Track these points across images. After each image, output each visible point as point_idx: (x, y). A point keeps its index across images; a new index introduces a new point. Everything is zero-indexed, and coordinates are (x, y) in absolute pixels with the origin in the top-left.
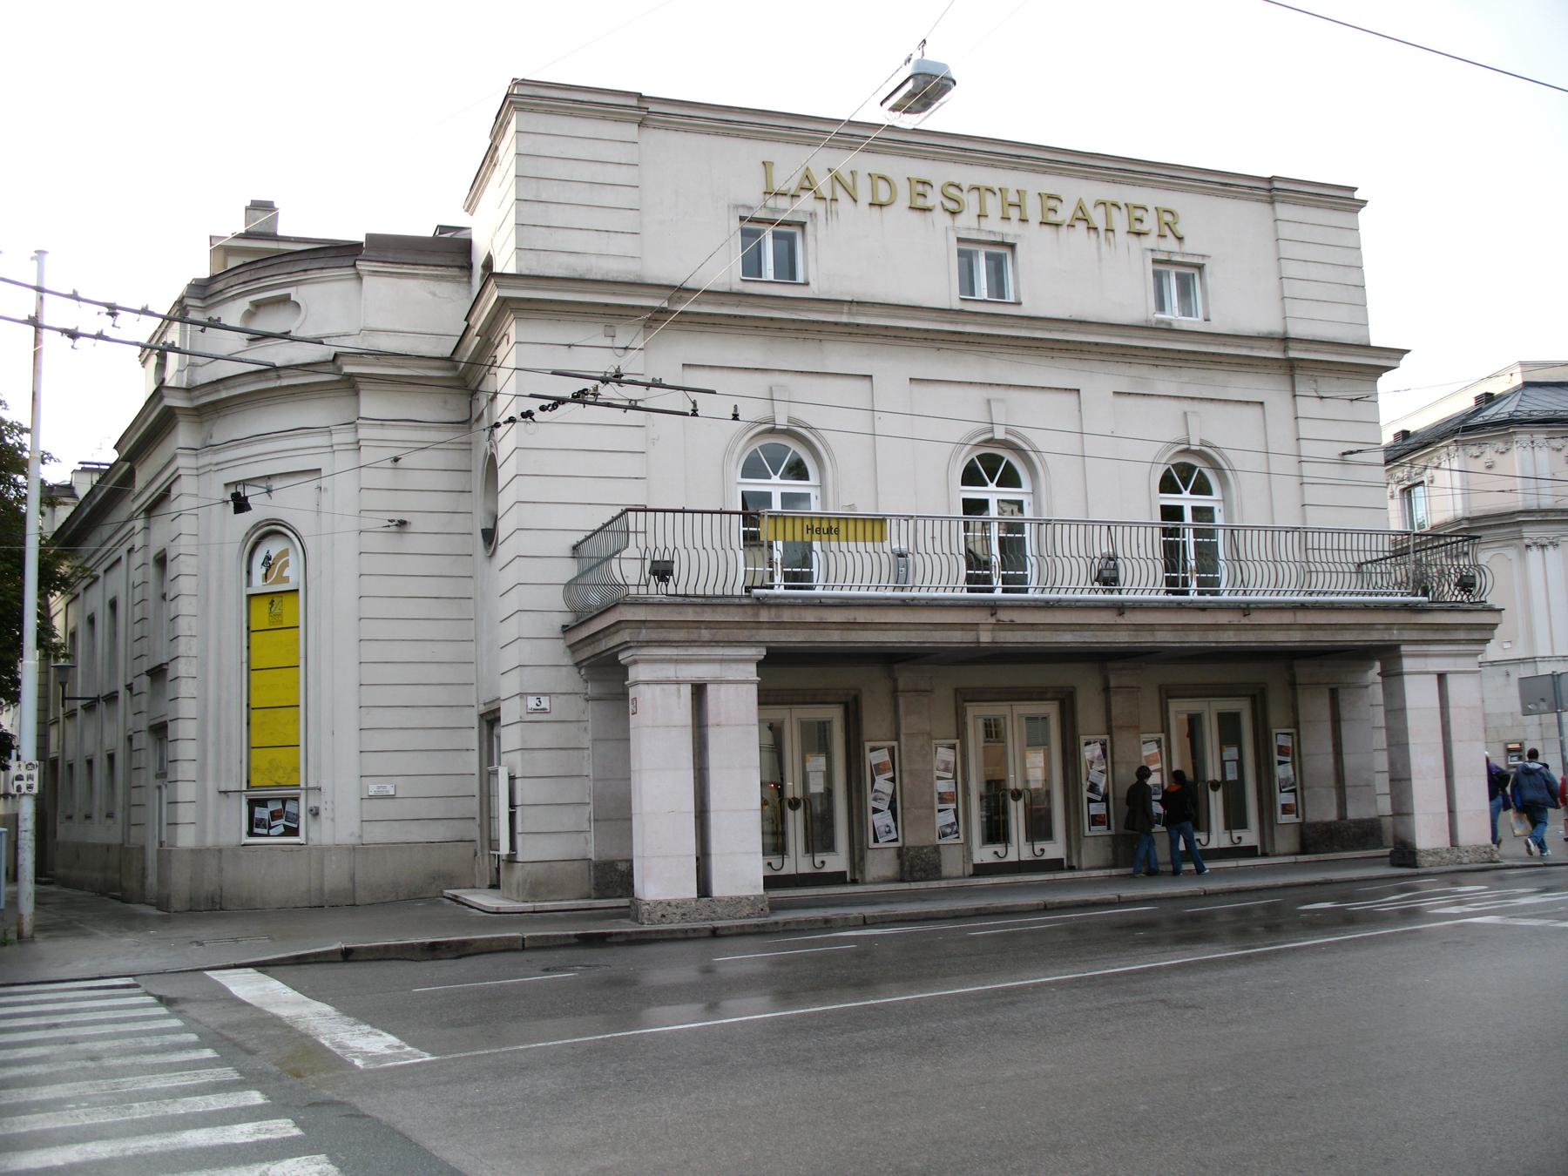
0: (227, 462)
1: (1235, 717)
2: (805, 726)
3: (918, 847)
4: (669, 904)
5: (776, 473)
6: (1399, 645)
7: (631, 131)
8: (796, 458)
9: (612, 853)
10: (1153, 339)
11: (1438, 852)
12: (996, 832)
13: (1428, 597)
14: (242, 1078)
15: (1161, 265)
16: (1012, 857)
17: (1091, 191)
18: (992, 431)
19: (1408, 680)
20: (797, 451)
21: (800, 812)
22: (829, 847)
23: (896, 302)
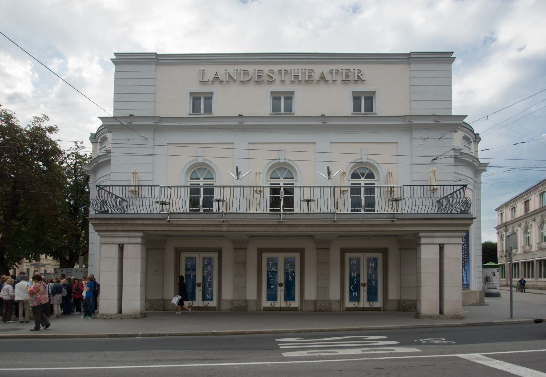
0: (103, 181)
1: (375, 260)
2: (369, 260)
4: (106, 315)
5: (363, 177)
6: (418, 233)
7: (153, 67)
8: (370, 172)
10: (427, 120)
11: (432, 317)
12: (272, 297)
15: (356, 98)
17: (325, 69)
18: (362, 159)
19: (423, 248)
20: (370, 169)
22: (293, 299)
23: (302, 115)
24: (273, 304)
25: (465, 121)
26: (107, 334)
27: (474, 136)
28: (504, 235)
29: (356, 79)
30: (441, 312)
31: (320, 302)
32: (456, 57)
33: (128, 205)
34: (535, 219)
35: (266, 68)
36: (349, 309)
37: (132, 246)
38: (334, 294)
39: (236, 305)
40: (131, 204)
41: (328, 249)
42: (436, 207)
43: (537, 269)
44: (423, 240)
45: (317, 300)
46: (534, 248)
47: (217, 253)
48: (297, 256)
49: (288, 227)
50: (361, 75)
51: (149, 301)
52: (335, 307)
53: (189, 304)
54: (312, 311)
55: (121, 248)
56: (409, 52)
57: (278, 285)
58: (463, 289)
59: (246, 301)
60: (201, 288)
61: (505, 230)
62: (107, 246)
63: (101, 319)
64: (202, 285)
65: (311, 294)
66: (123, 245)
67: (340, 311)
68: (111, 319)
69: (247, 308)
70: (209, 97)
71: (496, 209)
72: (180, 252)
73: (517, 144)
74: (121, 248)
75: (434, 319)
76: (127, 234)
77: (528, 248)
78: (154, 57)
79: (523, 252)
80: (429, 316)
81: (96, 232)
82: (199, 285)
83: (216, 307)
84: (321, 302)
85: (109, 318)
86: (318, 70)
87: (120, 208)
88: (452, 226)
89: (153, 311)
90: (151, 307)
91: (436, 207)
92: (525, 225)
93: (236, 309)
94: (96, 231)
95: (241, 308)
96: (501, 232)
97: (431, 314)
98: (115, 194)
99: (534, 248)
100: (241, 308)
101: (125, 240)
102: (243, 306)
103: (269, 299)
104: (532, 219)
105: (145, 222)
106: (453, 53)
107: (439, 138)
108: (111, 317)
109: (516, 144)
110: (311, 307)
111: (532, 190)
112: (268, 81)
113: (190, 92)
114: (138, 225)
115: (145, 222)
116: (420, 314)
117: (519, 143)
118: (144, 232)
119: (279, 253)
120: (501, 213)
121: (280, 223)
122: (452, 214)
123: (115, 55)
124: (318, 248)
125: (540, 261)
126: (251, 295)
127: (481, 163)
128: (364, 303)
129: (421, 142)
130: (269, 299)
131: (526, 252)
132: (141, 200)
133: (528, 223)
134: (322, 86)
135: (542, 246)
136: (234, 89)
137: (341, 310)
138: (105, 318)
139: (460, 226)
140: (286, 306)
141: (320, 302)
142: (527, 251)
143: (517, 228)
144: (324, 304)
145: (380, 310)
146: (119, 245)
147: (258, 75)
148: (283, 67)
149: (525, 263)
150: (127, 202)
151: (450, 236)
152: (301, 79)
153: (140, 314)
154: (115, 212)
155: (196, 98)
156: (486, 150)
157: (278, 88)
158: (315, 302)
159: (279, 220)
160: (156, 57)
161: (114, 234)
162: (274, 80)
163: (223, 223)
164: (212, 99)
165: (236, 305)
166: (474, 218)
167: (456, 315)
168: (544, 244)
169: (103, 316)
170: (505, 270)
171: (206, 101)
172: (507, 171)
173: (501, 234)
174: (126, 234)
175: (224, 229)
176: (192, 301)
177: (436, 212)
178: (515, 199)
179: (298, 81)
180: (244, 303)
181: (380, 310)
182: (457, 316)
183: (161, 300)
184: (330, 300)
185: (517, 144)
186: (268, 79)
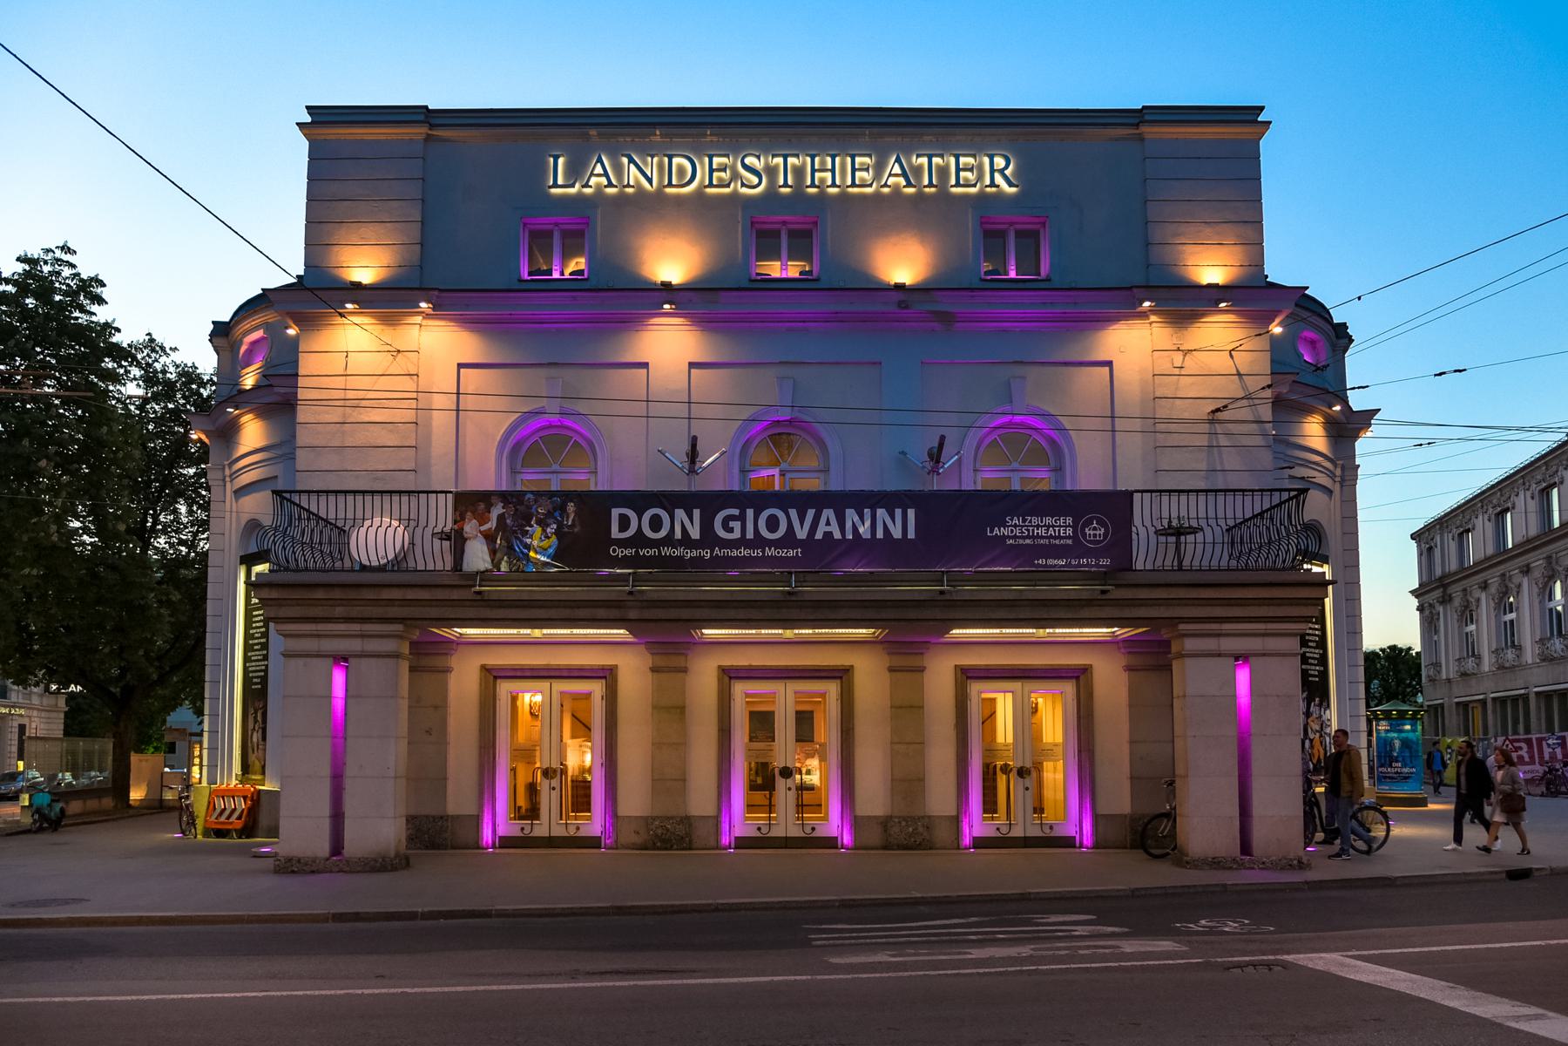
11: (1219, 862)
25: (1306, 292)
26: (332, 911)
27: (1332, 334)
28: (1439, 614)
30: (1246, 847)
31: (900, 822)
32: (1270, 122)
34: (1486, 582)
37: (373, 661)
39: (659, 831)
42: (1226, 546)
43: (1539, 719)
45: (891, 817)
46: (1530, 654)
54: (877, 849)
56: (1140, 107)
58: (775, 693)
59: (687, 820)
61: (1441, 599)
62: (301, 662)
63: (283, 873)
68: (313, 872)
69: (690, 841)
71: (1412, 535)
73: (1444, 373)
75: (1224, 868)
77: (1510, 654)
78: (422, 117)
79: (1498, 669)
80: (1210, 860)
83: (600, 837)
84: (904, 823)
91: (1226, 546)
92: (1500, 584)
93: (659, 844)
95: (674, 841)
96: (1431, 606)
97: (1217, 855)
98: (316, 513)
99: (1530, 654)
100: (674, 841)
104: (1519, 568)
105: (411, 594)
106: (1262, 109)
108: (313, 869)
109: (1440, 374)
111: (1517, 477)
116: (1187, 856)
120: (1427, 546)
121: (788, 598)
123: (311, 111)
125: (1546, 697)
127: (1354, 410)
131: (1506, 668)
133: (1510, 580)
135: (1553, 648)
138: (296, 869)
139: (1292, 605)
141: (900, 822)
142: (1507, 665)
143: (1477, 593)
144: (911, 829)
149: (1502, 701)
150: (344, 531)
151: (1263, 631)
156: (1359, 388)
160: (427, 117)
161: (321, 627)
163: (630, 598)
165: (659, 831)
167: (1286, 859)
168: (1557, 645)
169: (289, 864)
170: (1447, 722)
172: (1421, 445)
173: (1431, 612)
174: (356, 627)
178: (1466, 507)
180: (681, 826)
182: (1291, 860)
184: (929, 817)
185: (1444, 373)
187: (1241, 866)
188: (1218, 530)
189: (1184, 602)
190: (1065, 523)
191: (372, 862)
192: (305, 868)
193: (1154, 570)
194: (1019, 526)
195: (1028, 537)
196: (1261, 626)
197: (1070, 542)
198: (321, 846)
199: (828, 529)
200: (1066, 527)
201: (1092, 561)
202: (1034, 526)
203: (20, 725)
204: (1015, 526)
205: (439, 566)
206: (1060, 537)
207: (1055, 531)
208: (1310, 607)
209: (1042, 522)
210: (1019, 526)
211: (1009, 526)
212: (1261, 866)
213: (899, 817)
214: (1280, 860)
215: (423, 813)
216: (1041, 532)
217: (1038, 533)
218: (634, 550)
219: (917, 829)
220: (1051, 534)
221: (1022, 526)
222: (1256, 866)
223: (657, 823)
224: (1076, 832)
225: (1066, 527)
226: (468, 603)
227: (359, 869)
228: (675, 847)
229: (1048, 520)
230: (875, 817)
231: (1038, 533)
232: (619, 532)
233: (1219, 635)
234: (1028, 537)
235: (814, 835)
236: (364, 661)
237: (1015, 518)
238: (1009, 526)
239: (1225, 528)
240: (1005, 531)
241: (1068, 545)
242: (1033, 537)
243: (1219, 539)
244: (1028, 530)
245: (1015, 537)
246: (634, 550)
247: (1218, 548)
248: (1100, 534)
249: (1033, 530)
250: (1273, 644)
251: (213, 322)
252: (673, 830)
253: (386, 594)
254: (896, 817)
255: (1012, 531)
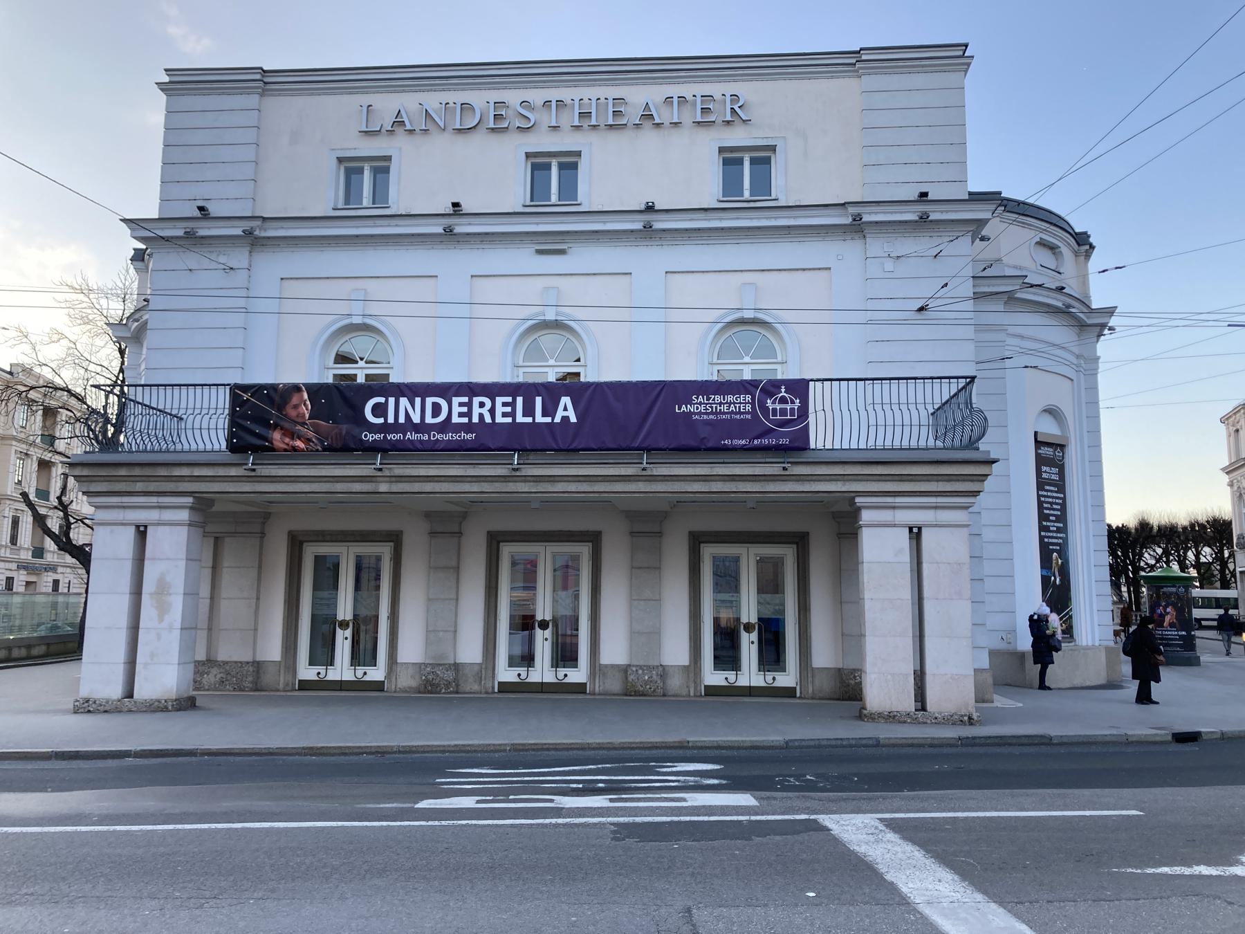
2: (761, 562)
3: (241, 662)
7: (253, 100)
9: (851, 664)
11: (895, 716)
12: (727, 656)
13: (309, 419)
14: (616, 829)
15: (730, 159)
16: (743, 681)
21: (548, 633)
22: (373, 662)
24: (523, 676)
29: (729, 118)
31: (637, 670)
33: (183, 427)
35: (513, 97)
36: (712, 691)
37: (167, 528)
38: (675, 652)
40: (189, 425)
41: (659, 534)
44: (866, 516)
45: (629, 665)
47: (590, 544)
48: (385, 550)
49: (534, 481)
50: (739, 107)
51: (220, 665)
52: (675, 683)
53: (319, 673)
54: (618, 695)
55: (142, 533)
57: (742, 627)
59: (457, 667)
60: (348, 633)
64: (351, 625)
65: (615, 651)
66: (146, 527)
67: (690, 695)
68: (106, 711)
69: (457, 685)
70: (382, 167)
72: (498, 542)
73: (1106, 270)
74: (142, 533)
75: (900, 722)
76: (156, 501)
78: (258, 77)
81: (85, 498)
82: (344, 625)
83: (586, 683)
84: (640, 672)
85: (102, 708)
86: (639, 95)
87: (155, 433)
88: (937, 481)
89: (230, 691)
90: (223, 682)
94: (84, 493)
97: (893, 710)
98: (149, 404)
101: (153, 515)
102: (447, 681)
103: (512, 663)
105: (197, 472)
107: (935, 256)
108: (107, 708)
109: (1104, 271)
110: (614, 684)
112: (518, 127)
113: (526, 153)
114: (181, 478)
115: (197, 472)
117: (1112, 269)
118: (197, 495)
119: (542, 544)
122: (140, 452)
124: (840, 534)
126: (470, 651)
128: (750, 674)
129: (889, 265)
130: (512, 663)
132: (199, 417)
134: (649, 136)
136: (441, 146)
137: (692, 694)
138: (92, 709)
139: (958, 480)
140: (555, 681)
144: (646, 678)
145: (794, 696)
146: (138, 527)
147: (702, 109)
148: (554, 94)
150: (181, 419)
151: (935, 505)
152: (556, 123)
153: (176, 700)
154: (139, 446)
155: (351, 167)
157: (737, 137)
158: (625, 670)
159: (510, 466)
161: (126, 499)
162: (534, 124)
163: (379, 474)
164: (389, 173)
165: (430, 677)
166: (994, 462)
171: (561, 171)
175: (383, 487)
176: (526, 669)
177: (931, 443)
179: (653, 124)
181: (794, 696)
182: (962, 716)
183: (248, 663)
185: (1106, 270)
186: (518, 124)
187: (916, 721)
188: (924, 413)
189: (860, 477)
190: (745, 400)
191: (157, 703)
192: (99, 708)
193: (867, 449)
194: (703, 404)
195: (712, 413)
196: (933, 500)
197: (749, 417)
198: (114, 691)
199: (565, 414)
200: (746, 403)
201: (772, 441)
202: (717, 404)
203: (54, 580)
204: (700, 404)
205: (217, 447)
206: (740, 413)
207: (735, 407)
208: (976, 483)
209: (724, 400)
210: (704, 403)
211: (695, 404)
212: (933, 721)
213: (637, 666)
214: (952, 716)
215: (235, 659)
216: (724, 408)
217: (720, 410)
218: (382, 435)
219: (652, 677)
220: (732, 410)
221: (707, 404)
222: (929, 722)
223: (429, 669)
224: (797, 685)
225: (746, 403)
226: (244, 479)
227: (144, 709)
228: (443, 691)
229: (730, 398)
230: (618, 666)
231: (720, 410)
232: (432, 418)
233: (894, 508)
234: (712, 413)
235: (566, 680)
236: (161, 528)
237: (701, 397)
238: (695, 404)
239: (931, 411)
240: (691, 408)
241: (748, 419)
242: (716, 413)
243: (924, 421)
244: (712, 407)
245: (700, 413)
246: (382, 435)
247: (924, 430)
248: (792, 409)
249: (716, 407)
250: (168, 515)
251: (135, 249)
252: (442, 676)
253: (177, 472)
254: (633, 666)
255: (697, 408)
